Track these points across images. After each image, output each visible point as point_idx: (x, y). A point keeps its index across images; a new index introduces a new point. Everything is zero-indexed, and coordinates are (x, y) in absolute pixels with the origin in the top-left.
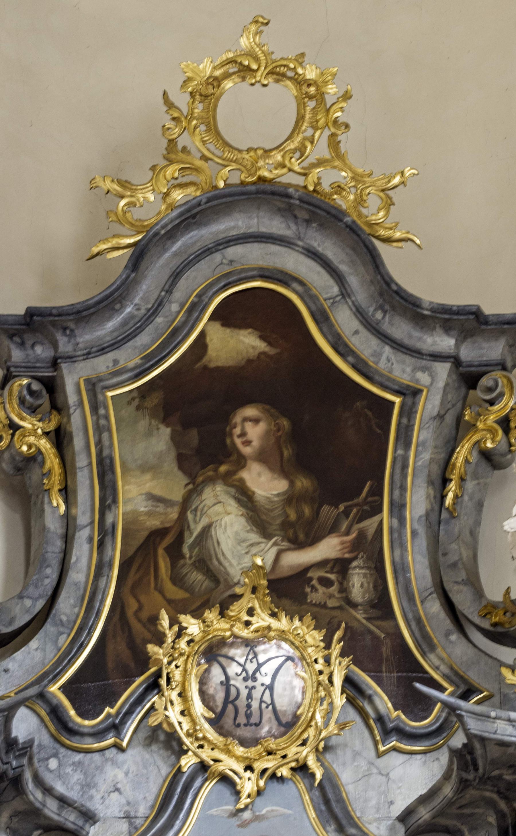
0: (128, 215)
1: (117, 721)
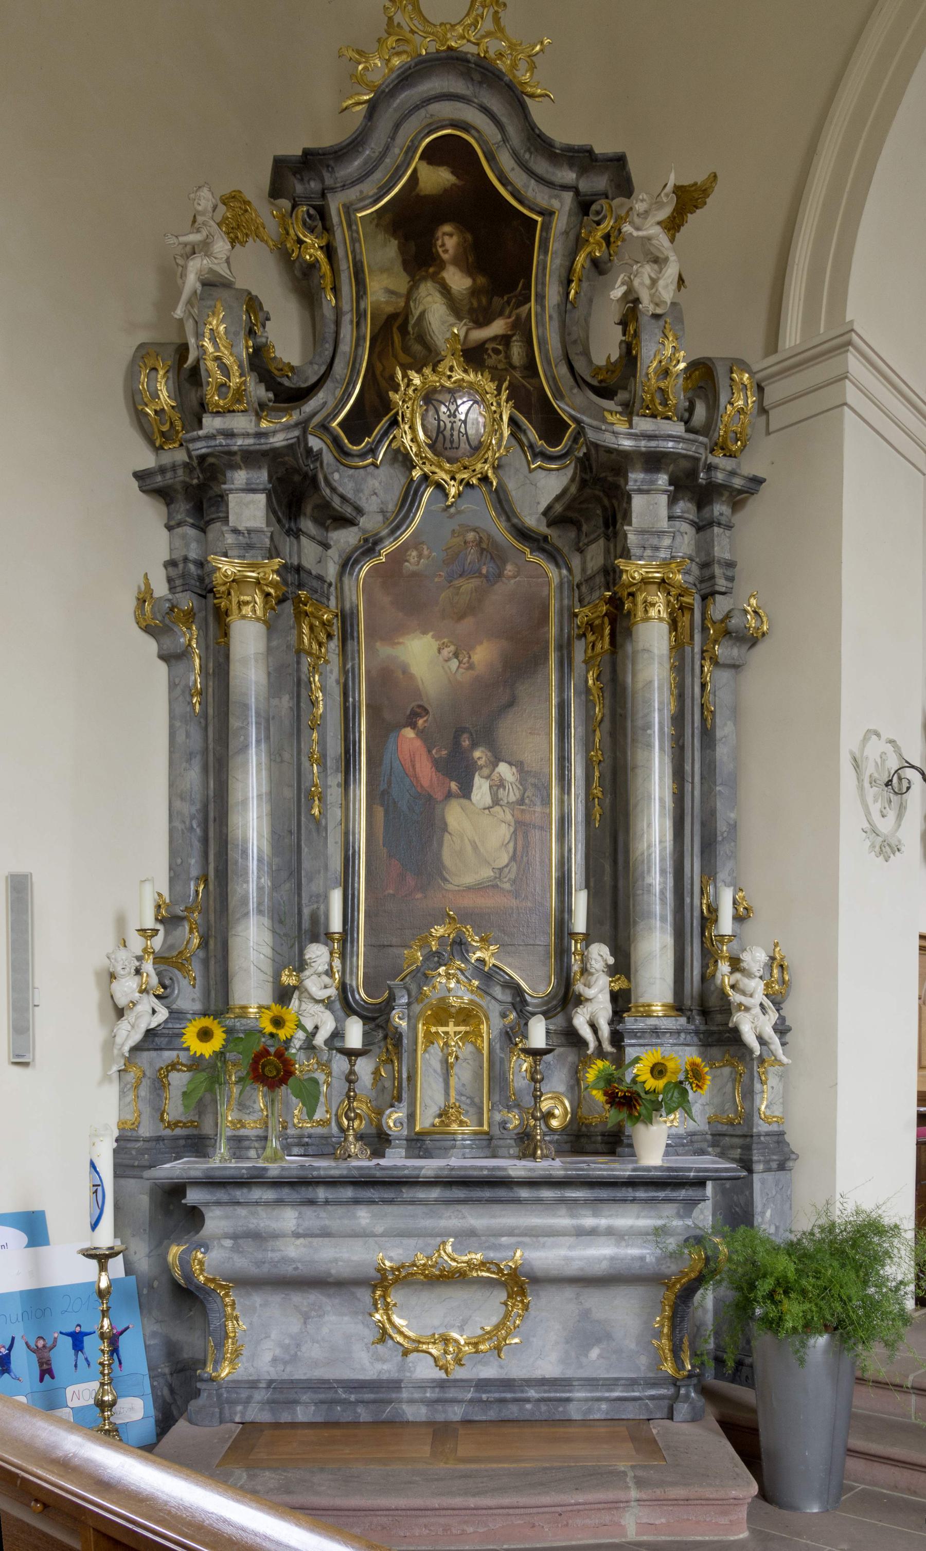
0: (364, 78)
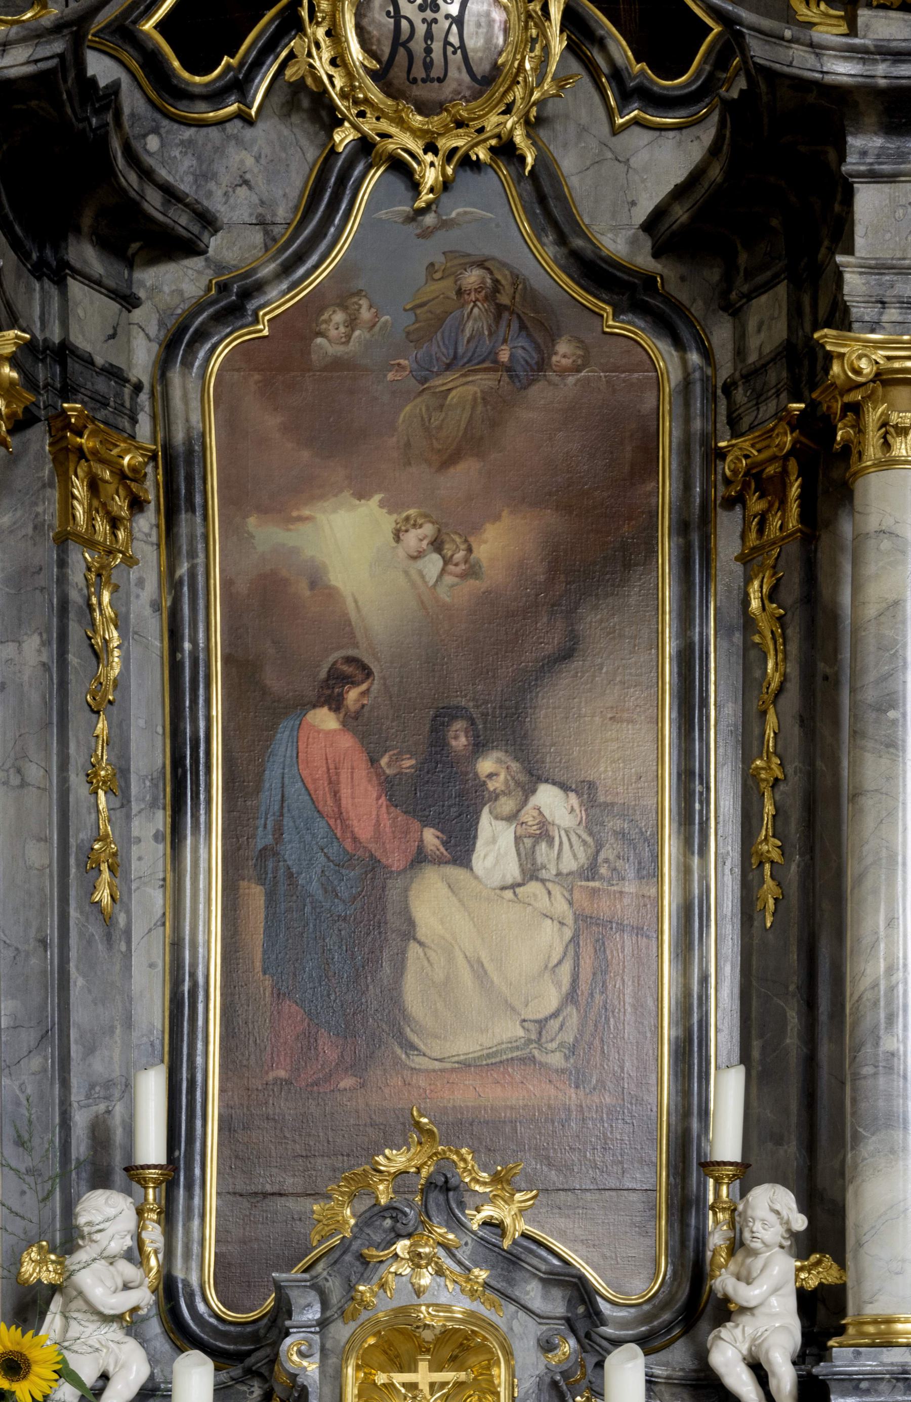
1: (241, 76)
